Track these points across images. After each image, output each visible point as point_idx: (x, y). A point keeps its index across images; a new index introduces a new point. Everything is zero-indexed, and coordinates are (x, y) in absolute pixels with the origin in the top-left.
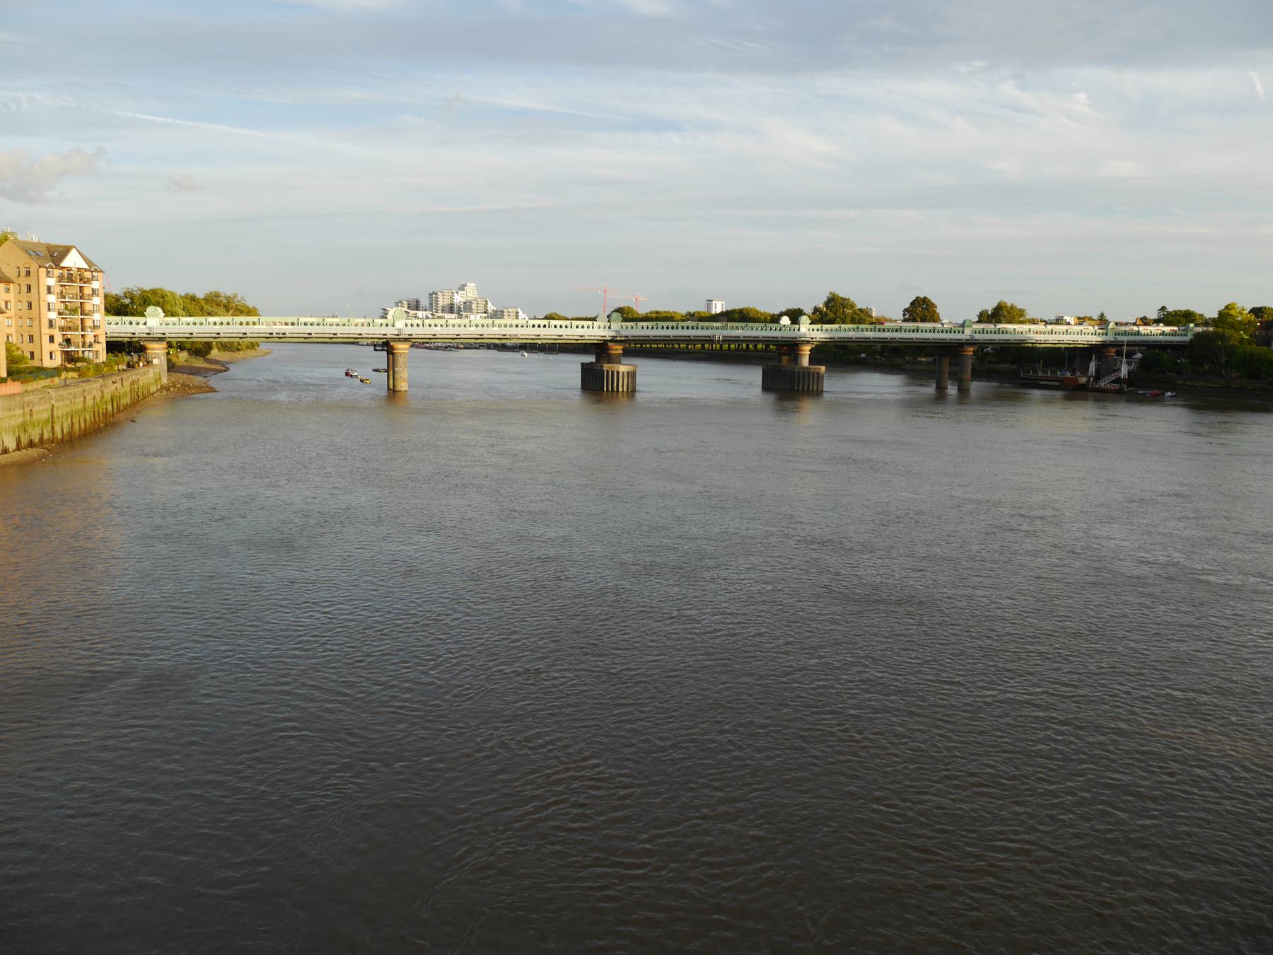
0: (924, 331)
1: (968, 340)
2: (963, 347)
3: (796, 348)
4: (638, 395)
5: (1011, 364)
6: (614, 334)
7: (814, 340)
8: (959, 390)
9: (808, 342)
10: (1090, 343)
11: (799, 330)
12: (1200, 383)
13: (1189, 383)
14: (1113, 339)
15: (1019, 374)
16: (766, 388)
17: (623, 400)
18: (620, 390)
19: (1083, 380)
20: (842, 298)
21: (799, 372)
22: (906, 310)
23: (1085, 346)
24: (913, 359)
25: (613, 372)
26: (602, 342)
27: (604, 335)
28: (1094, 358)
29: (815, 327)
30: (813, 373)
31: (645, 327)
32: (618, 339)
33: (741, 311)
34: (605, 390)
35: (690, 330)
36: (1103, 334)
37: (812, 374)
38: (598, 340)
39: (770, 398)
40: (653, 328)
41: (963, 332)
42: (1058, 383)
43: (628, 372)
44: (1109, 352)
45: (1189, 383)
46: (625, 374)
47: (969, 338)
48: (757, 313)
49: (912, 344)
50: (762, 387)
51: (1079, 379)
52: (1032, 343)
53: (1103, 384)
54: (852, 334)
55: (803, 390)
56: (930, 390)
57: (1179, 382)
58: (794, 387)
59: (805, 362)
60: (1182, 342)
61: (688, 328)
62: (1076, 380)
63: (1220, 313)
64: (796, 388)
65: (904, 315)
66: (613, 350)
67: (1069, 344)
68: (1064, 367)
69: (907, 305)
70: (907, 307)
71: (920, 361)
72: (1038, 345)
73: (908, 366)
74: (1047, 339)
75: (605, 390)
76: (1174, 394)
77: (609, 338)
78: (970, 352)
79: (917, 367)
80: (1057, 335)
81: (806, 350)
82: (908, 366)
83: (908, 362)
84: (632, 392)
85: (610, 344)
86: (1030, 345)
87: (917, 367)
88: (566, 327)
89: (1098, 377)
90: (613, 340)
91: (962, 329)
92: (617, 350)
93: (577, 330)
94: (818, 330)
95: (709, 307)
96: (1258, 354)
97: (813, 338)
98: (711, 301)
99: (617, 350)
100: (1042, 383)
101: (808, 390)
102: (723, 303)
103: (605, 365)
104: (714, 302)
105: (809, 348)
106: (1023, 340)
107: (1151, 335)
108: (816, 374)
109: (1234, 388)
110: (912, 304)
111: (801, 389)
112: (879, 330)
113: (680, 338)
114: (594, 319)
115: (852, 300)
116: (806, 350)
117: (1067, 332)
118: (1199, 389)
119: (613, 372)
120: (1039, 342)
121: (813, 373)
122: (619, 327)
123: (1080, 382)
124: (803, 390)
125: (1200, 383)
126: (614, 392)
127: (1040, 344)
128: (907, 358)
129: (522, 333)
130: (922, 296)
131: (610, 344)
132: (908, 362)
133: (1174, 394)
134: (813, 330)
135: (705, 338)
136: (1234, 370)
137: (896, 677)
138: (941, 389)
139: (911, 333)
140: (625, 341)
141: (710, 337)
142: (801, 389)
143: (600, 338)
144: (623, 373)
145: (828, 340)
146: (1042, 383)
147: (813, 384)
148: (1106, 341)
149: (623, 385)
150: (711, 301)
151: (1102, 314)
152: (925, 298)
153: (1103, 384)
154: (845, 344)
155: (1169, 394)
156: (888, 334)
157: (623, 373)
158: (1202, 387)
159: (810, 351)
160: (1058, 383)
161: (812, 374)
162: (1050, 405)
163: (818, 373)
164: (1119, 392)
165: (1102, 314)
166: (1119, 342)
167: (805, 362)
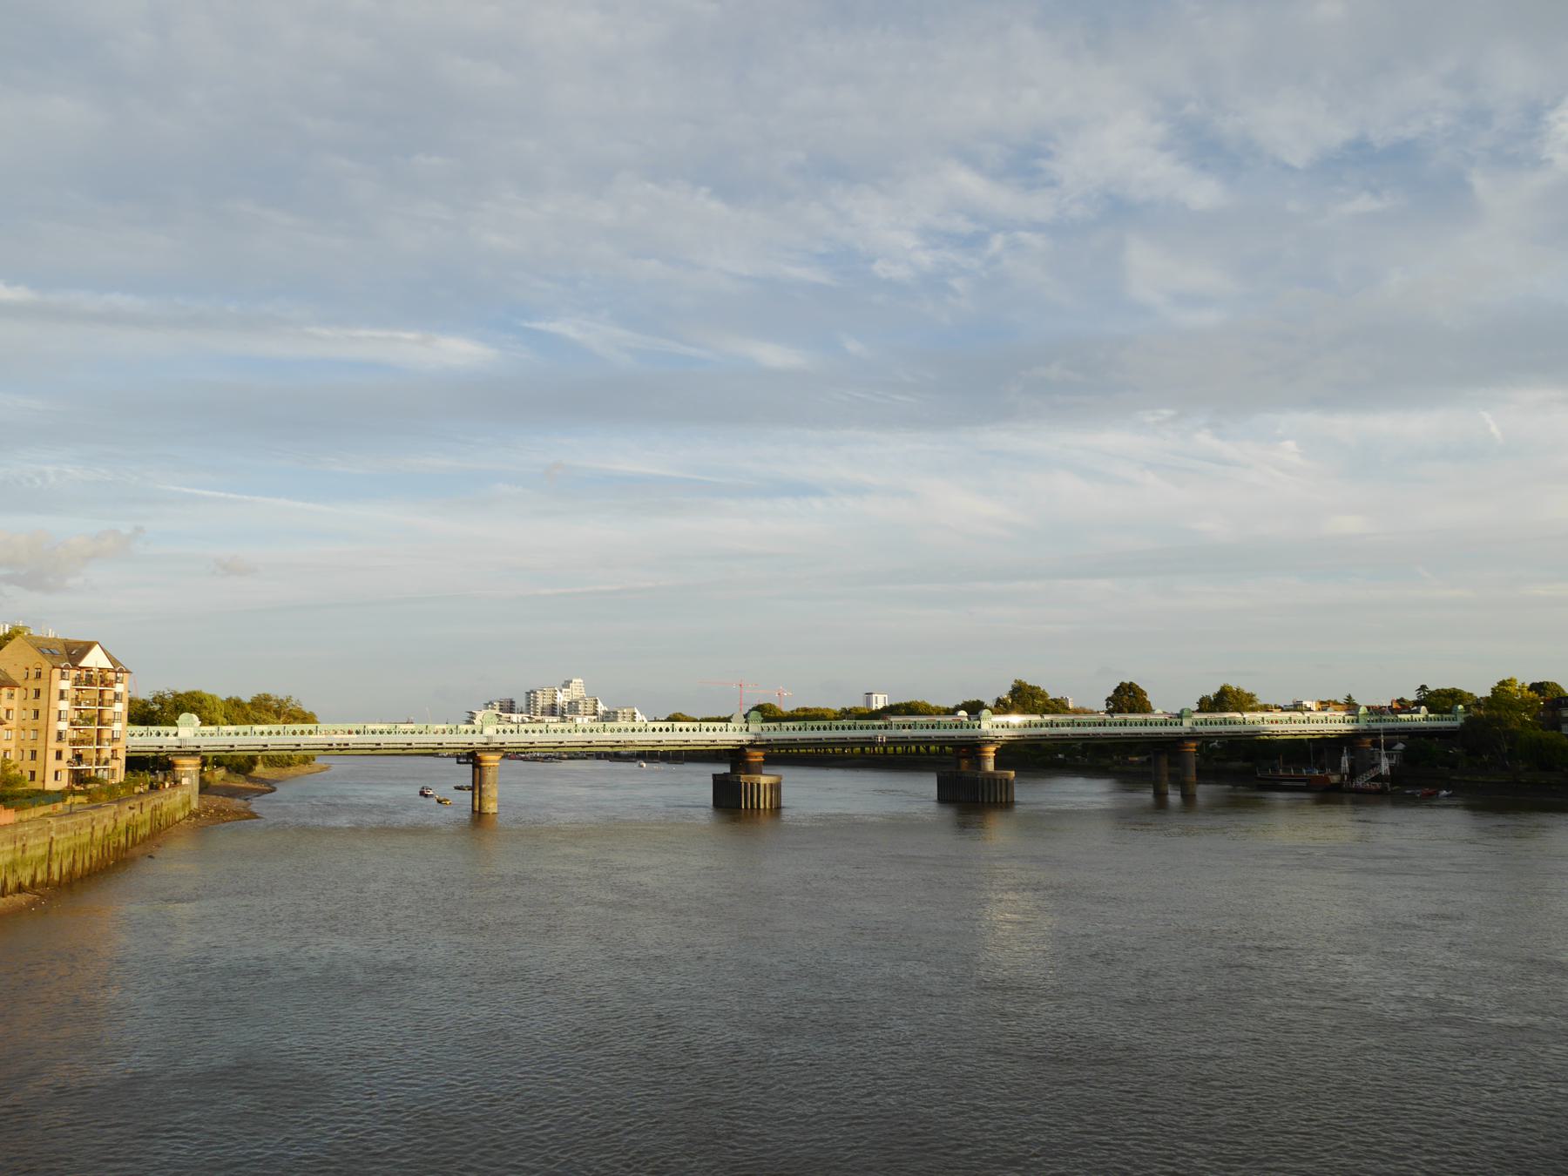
0: (1131, 724)
2: (1183, 743)
3: (977, 749)
4: (786, 814)
6: (753, 737)
10: (1339, 732)
11: (979, 727)
12: (1480, 779)
13: (1467, 778)
14: (1366, 727)
15: (1256, 773)
16: (943, 798)
18: (762, 806)
19: (1335, 779)
22: (1109, 699)
23: (1333, 736)
25: (752, 784)
28: (1345, 751)
32: (758, 743)
38: (733, 745)
39: (949, 813)
41: (1181, 724)
42: (1304, 784)
43: (771, 785)
47: (1189, 730)
51: (1330, 777)
52: (1268, 735)
53: (1360, 782)
56: (1147, 796)
59: (990, 766)
62: (1327, 778)
63: (1493, 690)
64: (980, 800)
65: (1108, 705)
69: (1110, 693)
70: (1110, 695)
76: (1450, 792)
77: (747, 743)
78: (1191, 748)
80: (1297, 724)
81: (990, 751)
82: (1116, 768)
84: (777, 809)
85: (748, 750)
88: (694, 730)
89: (1353, 774)
90: (752, 745)
93: (708, 733)
95: (869, 701)
97: (997, 737)
98: (871, 694)
99: (756, 757)
102: (886, 696)
105: (994, 749)
110: (1117, 691)
111: (986, 800)
112: (812, 729)
114: (727, 720)
115: (1042, 689)
116: (990, 751)
119: (752, 784)
120: (1276, 733)
121: (1001, 780)
125: (1480, 779)
126: (755, 811)
127: (1277, 735)
128: (1115, 757)
131: (748, 750)
133: (1450, 792)
138: (1160, 796)
140: (767, 746)
143: (736, 743)
144: (765, 785)
149: (765, 802)
150: (871, 694)
151: (1349, 697)
152: (1131, 683)
153: (1360, 782)
158: (1484, 782)
159: (995, 752)
160: (1304, 784)
161: (998, 782)
166: (1197, 733)
167: (990, 766)
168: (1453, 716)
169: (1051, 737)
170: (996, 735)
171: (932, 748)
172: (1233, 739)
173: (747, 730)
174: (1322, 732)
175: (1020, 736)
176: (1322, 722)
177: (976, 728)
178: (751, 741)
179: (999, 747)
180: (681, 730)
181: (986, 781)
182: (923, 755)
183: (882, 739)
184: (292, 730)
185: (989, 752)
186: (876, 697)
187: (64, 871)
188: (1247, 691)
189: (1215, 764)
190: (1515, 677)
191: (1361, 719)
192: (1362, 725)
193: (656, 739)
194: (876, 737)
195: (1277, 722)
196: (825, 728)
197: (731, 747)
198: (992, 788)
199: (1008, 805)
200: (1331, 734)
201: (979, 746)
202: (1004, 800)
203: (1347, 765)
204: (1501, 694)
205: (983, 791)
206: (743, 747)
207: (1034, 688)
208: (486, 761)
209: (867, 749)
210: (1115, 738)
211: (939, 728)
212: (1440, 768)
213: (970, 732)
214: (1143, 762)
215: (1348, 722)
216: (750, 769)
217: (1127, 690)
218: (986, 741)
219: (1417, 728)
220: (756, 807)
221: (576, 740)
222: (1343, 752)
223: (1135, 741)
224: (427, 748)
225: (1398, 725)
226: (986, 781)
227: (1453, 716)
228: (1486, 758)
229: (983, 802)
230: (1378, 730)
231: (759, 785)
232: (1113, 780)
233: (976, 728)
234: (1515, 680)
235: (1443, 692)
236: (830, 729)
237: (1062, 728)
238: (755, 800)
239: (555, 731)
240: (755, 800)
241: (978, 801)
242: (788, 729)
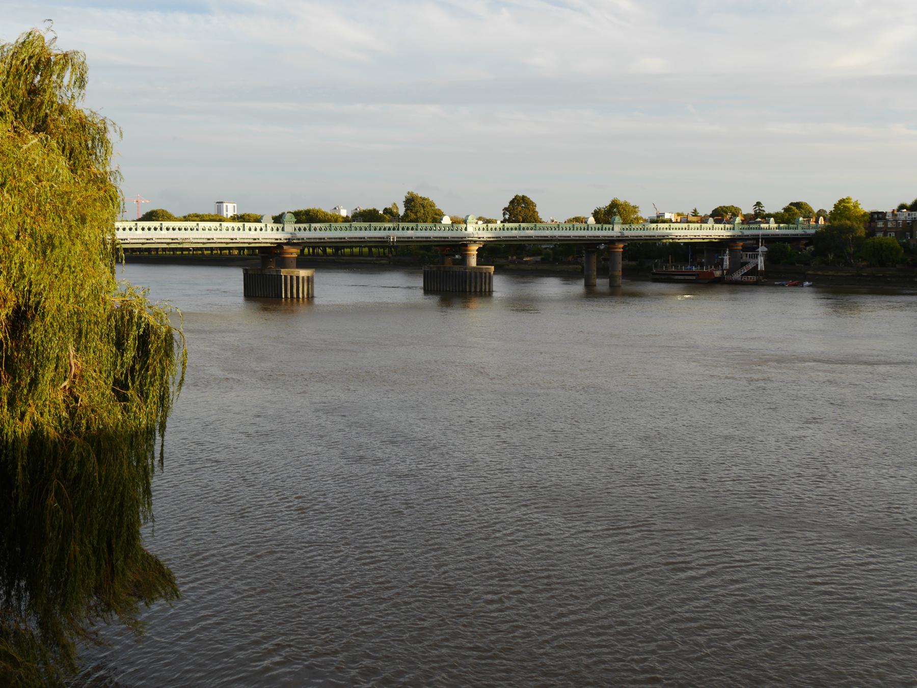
0: (525, 231)
1: (619, 237)
2: (614, 244)
3: (463, 248)
4: (317, 301)
5: (629, 261)
6: (289, 236)
7: (481, 239)
8: (586, 285)
9: (475, 242)
10: (721, 237)
11: (466, 229)
12: (830, 273)
13: (819, 273)
14: (740, 234)
15: (652, 270)
16: (427, 291)
17: (303, 309)
18: (301, 296)
19: (718, 273)
20: (421, 198)
21: (470, 273)
22: (505, 209)
23: (716, 240)
24: (517, 258)
25: (291, 277)
26: (275, 245)
27: (277, 237)
28: (727, 252)
29: (302, 226)
30: (485, 273)
31: (253, 229)
32: (295, 241)
33: (307, 213)
34: (283, 297)
35: (510, 231)
36: (730, 229)
37: (484, 274)
38: (271, 243)
39: (434, 300)
40: (261, 230)
41: (613, 229)
42: (694, 278)
43: (308, 277)
44: (616, 248)
45: (819, 273)
46: (305, 278)
47: (619, 234)
48: (327, 215)
49: (449, 243)
50: (245, 295)
51: (714, 272)
52: (673, 239)
53: (737, 276)
54: (515, 233)
55: (476, 291)
56: (578, 287)
57: (809, 272)
58: (466, 289)
59: (473, 262)
60: (796, 235)
61: (385, 229)
62: (712, 273)
63: (836, 206)
64: (468, 290)
65: (504, 214)
66: (288, 253)
67: (704, 239)
68: (668, 261)
69: (507, 205)
70: (507, 206)
71: (525, 261)
72: (677, 241)
73: (511, 266)
74: (187, 237)
75: (283, 297)
76: (811, 283)
77: (285, 241)
78: (620, 248)
79: (522, 267)
80: (693, 231)
81: (474, 249)
82: (511, 266)
83: (513, 262)
84: (310, 298)
85: (285, 247)
86: (671, 241)
87: (522, 267)
88: (239, 229)
89: (731, 271)
90: (289, 243)
91: (465, 225)
92: (292, 254)
93: (251, 232)
94: (155, 229)
95: (220, 209)
96: (887, 243)
97: (479, 238)
98: (222, 202)
99: (292, 254)
100: (677, 277)
101: (481, 291)
102: (235, 205)
103: (282, 270)
104: (225, 205)
105: (477, 248)
106: (462, 238)
107: (769, 229)
108: (478, 275)
109: (864, 276)
110: (512, 202)
111: (473, 290)
112: (356, 229)
113: (355, 240)
114: (258, 220)
115: (853, 200)
116: (474, 249)
117: (559, 227)
118: (830, 278)
119: (291, 277)
120: (678, 237)
121: (485, 273)
122: (290, 228)
123: (716, 276)
124: (476, 291)
125: (830, 273)
126: (294, 300)
127: (679, 239)
128: (510, 257)
129: (194, 237)
130: (520, 195)
131: (285, 247)
132: (513, 262)
133: (811, 283)
134: (149, 229)
135: (380, 240)
136: (860, 260)
137: (585, 577)
138: (589, 286)
139: (338, 231)
140: (301, 244)
141: (383, 238)
142: (473, 290)
143: (274, 241)
144: (303, 277)
145: (491, 239)
146: (677, 277)
147: (485, 284)
148: (734, 236)
149: (303, 291)
150: (222, 202)
151: (695, 210)
152: (524, 197)
153: (737, 276)
154: (523, 243)
155: (807, 283)
156: (548, 232)
157: (303, 277)
158: (833, 275)
159: (477, 250)
160: (694, 278)
161: (484, 274)
162: (628, 300)
163: (481, 274)
164: (757, 284)
165: (695, 210)
166: (745, 236)
167: (473, 262)
168: (796, 226)
169: (520, 238)
170: (480, 236)
171: (329, 250)
172: (650, 242)
173: (283, 229)
174: (709, 237)
175: (496, 238)
176: (710, 229)
177: (463, 230)
178: (289, 239)
179: (481, 246)
180: (250, 229)
181: (473, 274)
182: (321, 256)
183: (394, 239)
184: (129, 227)
185: (473, 251)
186: (227, 206)
187: (823, 297)
188: (632, 204)
189: (603, 262)
190: (851, 197)
191: (736, 227)
192: (737, 232)
193: (229, 237)
194: (388, 237)
195: (679, 229)
196: (412, 229)
197: (269, 245)
198: (479, 280)
199: (486, 293)
200: (715, 239)
201: (466, 245)
202: (487, 290)
203: (728, 263)
204: (842, 209)
205: (476, 283)
206: (280, 246)
207: (424, 199)
208: (288, 253)
209: (373, 250)
210: (510, 240)
211: (573, 230)
212: (797, 265)
213: (454, 234)
214: (537, 262)
215: (727, 229)
216: (283, 263)
217: (521, 201)
218: (470, 241)
219: (774, 235)
220: (289, 296)
221: (163, 237)
222: (726, 253)
223: (595, 242)
224: (198, 243)
225: (761, 232)
226: (473, 274)
227: (796, 226)
228: (831, 257)
229: (470, 291)
230: (758, 235)
231: (298, 278)
232: (504, 277)
233: (463, 230)
234: (850, 199)
235: (725, 209)
236: (330, 230)
237: (527, 231)
238: (295, 291)
239: (124, 229)
240: (295, 291)
241: (466, 291)
242: (250, 229)
